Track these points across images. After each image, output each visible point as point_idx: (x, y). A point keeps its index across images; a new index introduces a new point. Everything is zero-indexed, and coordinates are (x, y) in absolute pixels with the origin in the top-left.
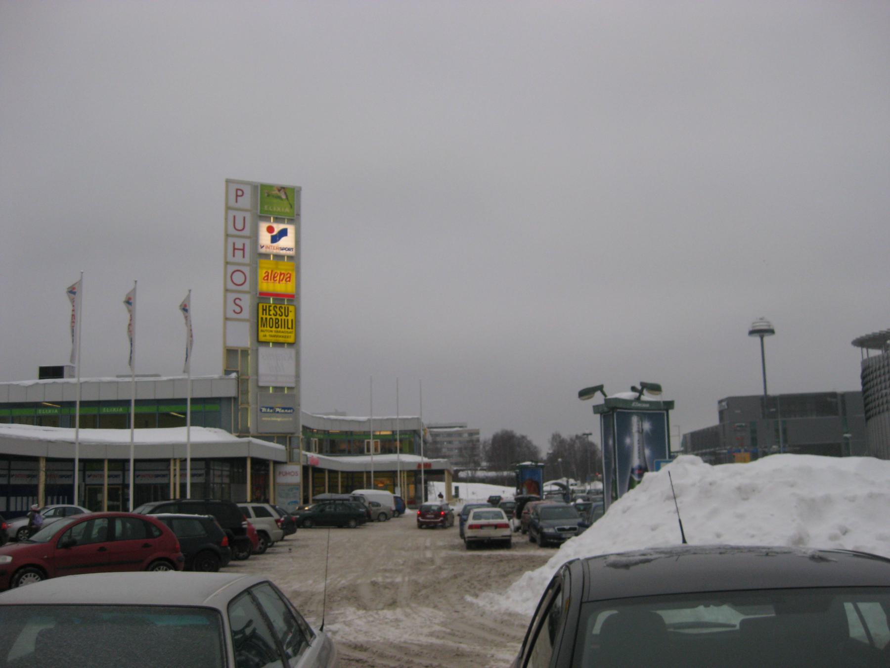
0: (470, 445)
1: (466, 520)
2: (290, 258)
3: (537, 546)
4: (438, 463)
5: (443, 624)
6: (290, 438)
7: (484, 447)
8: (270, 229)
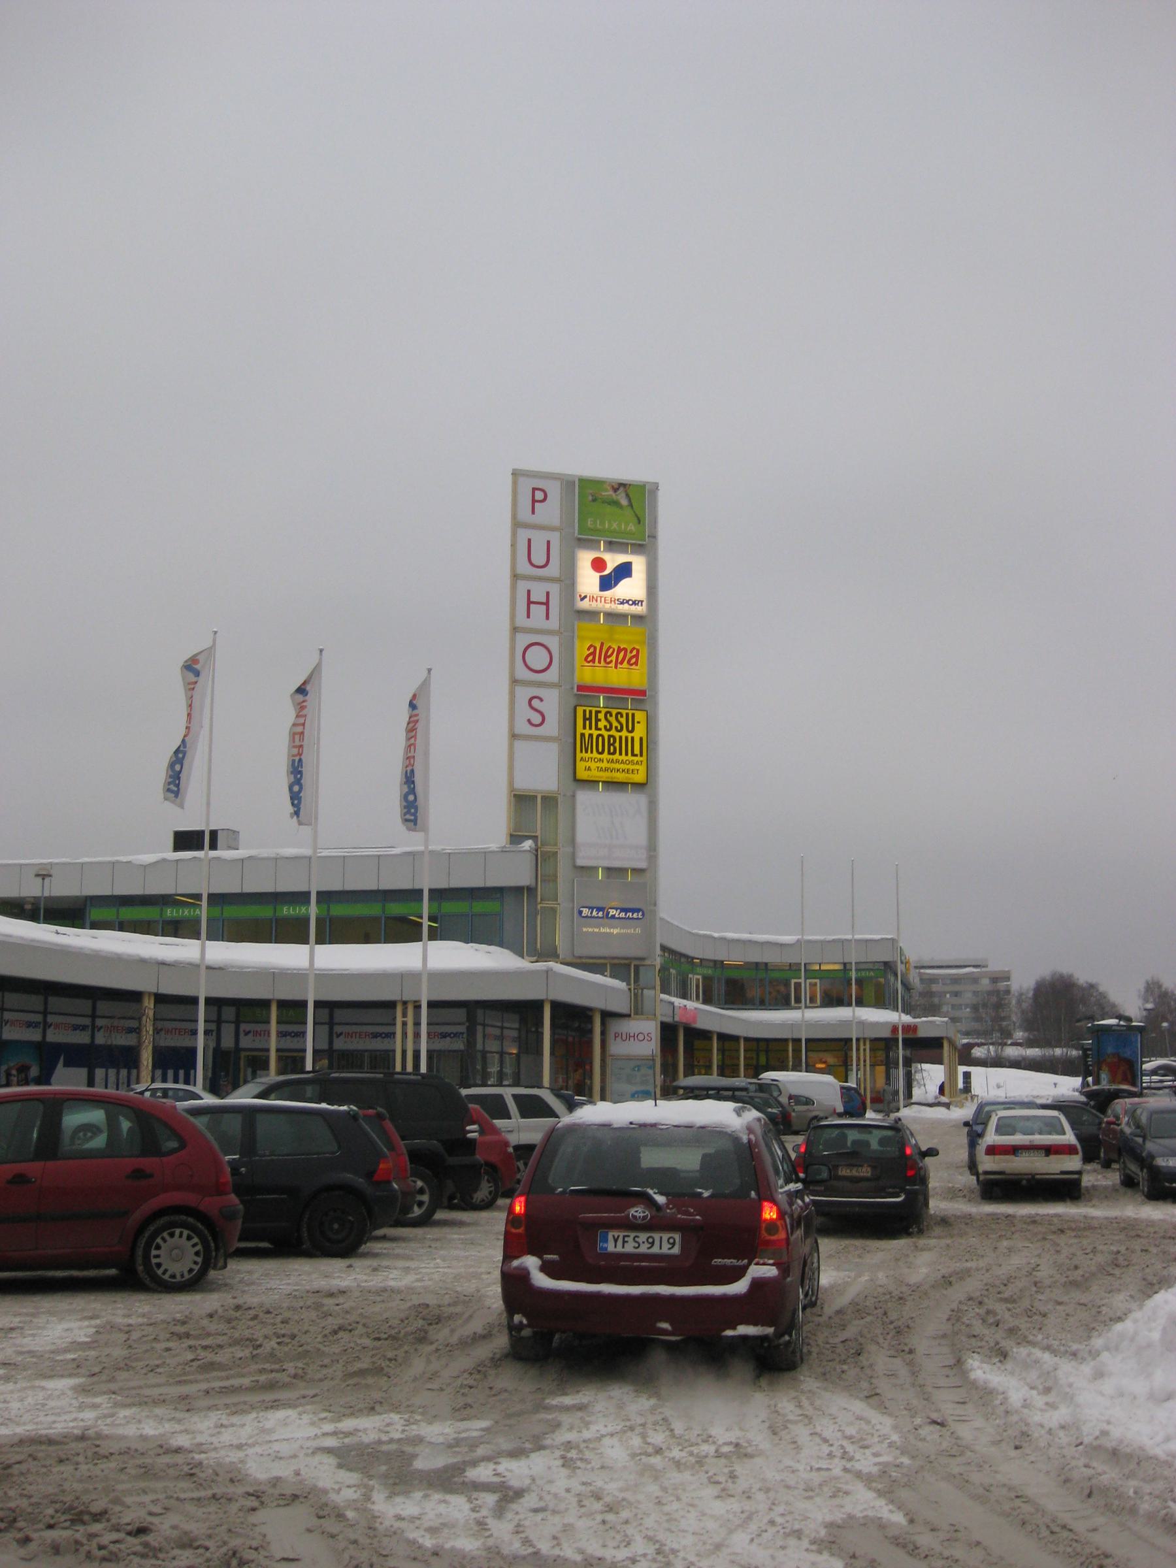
0: (994, 999)
1: (981, 1135)
2: (638, 618)
3: (1140, 1198)
4: (930, 1025)
5: (886, 1484)
6: (637, 968)
7: (1019, 1002)
8: (598, 564)
